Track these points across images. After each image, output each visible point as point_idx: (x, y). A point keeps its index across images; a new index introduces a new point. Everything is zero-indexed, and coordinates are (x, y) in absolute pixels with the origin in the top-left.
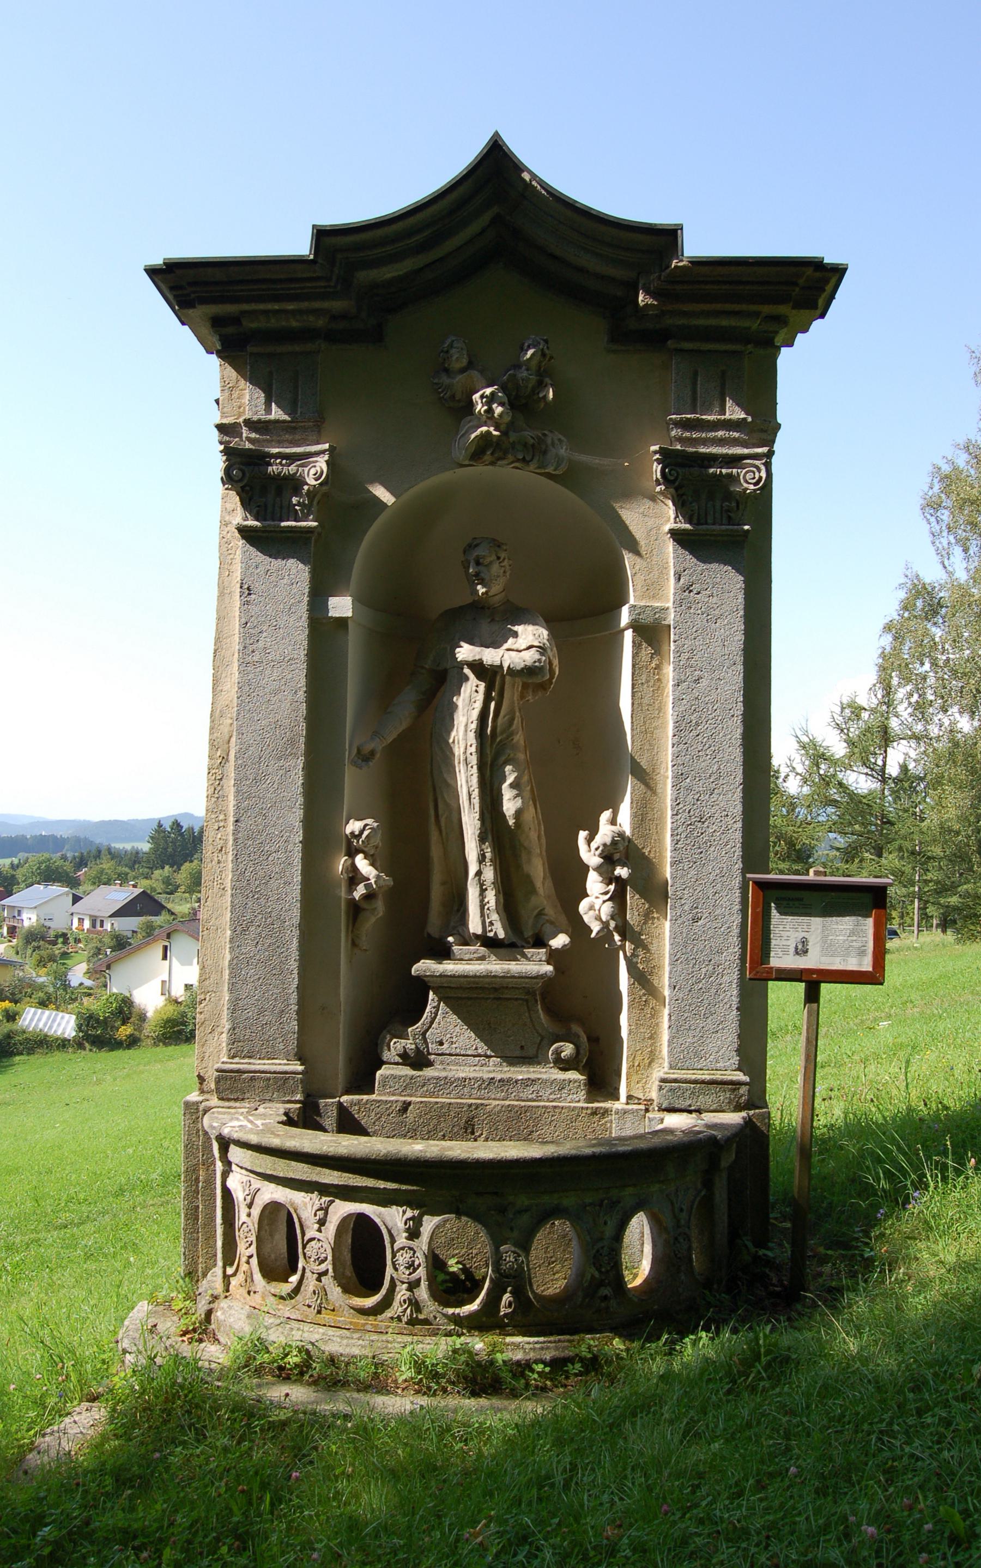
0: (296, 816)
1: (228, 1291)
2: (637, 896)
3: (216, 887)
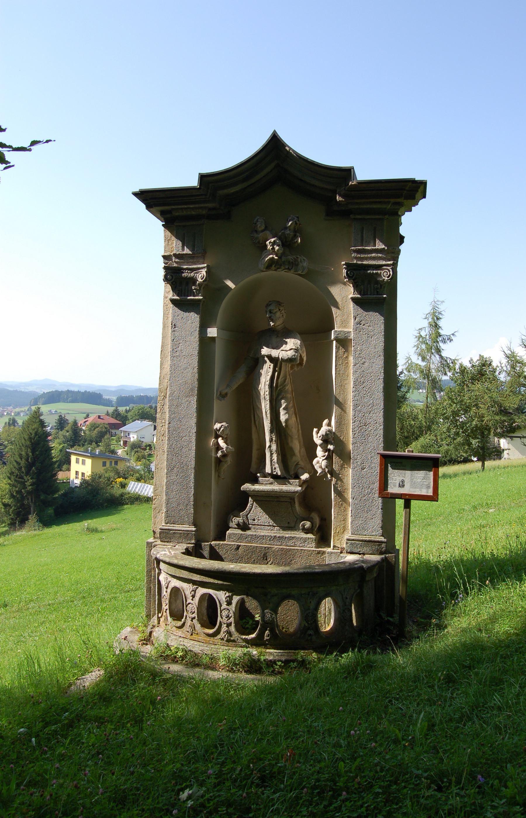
0: (193, 422)
1: (159, 624)
2: (338, 458)
3: (161, 451)
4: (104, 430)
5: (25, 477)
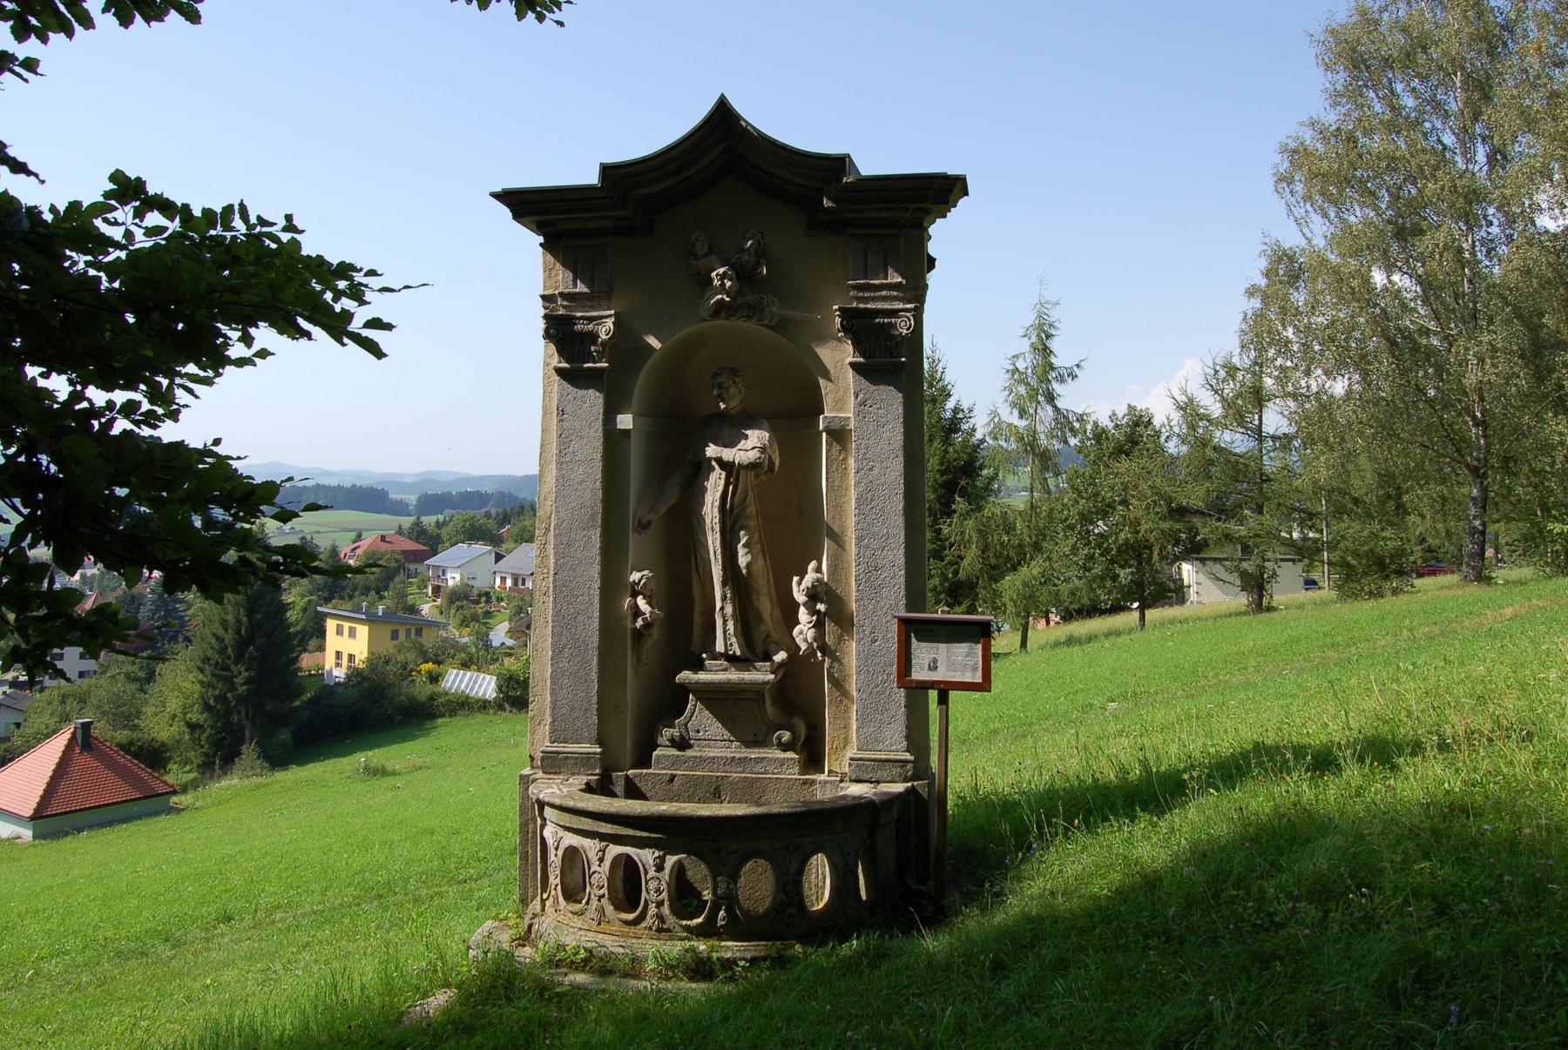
0: (595, 570)
4: (393, 564)
5: (233, 667)
